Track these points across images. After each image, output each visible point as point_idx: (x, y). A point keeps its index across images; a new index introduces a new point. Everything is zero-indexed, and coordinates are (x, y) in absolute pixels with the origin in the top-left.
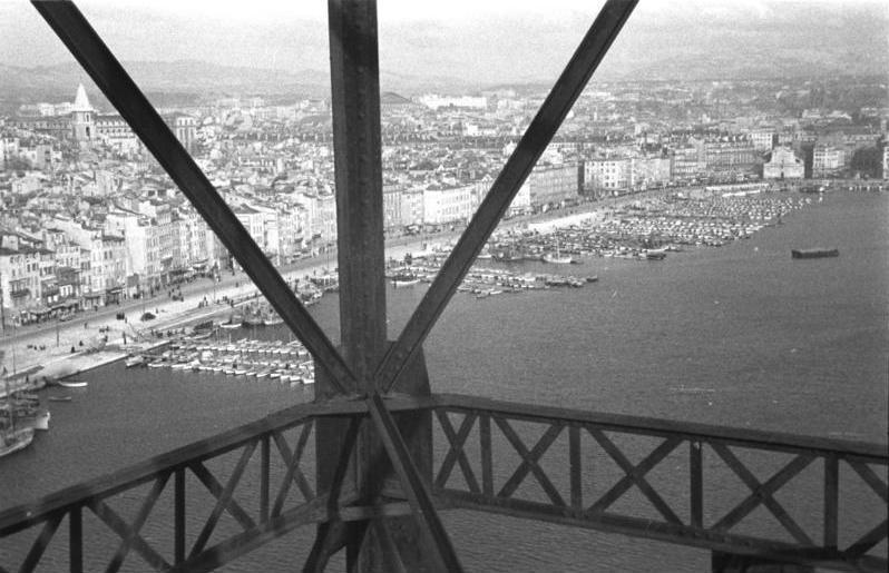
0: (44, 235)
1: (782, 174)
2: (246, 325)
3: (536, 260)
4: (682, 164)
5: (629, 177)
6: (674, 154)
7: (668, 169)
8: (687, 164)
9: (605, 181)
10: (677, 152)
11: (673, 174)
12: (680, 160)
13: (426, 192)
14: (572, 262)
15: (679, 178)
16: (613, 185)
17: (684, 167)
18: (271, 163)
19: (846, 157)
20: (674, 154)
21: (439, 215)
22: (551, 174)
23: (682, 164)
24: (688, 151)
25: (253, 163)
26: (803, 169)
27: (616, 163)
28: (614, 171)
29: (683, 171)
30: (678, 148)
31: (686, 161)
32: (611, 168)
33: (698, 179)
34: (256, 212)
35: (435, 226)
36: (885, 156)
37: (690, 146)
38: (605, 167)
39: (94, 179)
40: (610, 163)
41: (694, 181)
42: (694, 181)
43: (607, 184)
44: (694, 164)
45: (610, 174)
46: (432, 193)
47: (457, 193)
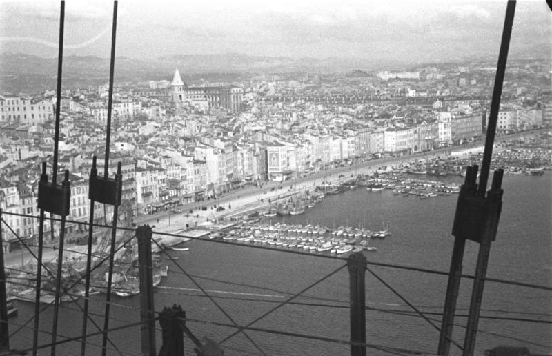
3: (456, 175)
5: (516, 122)
7: (541, 117)
10: (547, 105)
13: (386, 133)
16: (505, 127)
18: (289, 115)
20: (545, 107)
27: (507, 113)
28: (505, 118)
32: (503, 116)
34: (282, 145)
39: (185, 126)
40: (503, 113)
43: (501, 127)
45: (503, 120)
46: (390, 133)
47: (405, 133)
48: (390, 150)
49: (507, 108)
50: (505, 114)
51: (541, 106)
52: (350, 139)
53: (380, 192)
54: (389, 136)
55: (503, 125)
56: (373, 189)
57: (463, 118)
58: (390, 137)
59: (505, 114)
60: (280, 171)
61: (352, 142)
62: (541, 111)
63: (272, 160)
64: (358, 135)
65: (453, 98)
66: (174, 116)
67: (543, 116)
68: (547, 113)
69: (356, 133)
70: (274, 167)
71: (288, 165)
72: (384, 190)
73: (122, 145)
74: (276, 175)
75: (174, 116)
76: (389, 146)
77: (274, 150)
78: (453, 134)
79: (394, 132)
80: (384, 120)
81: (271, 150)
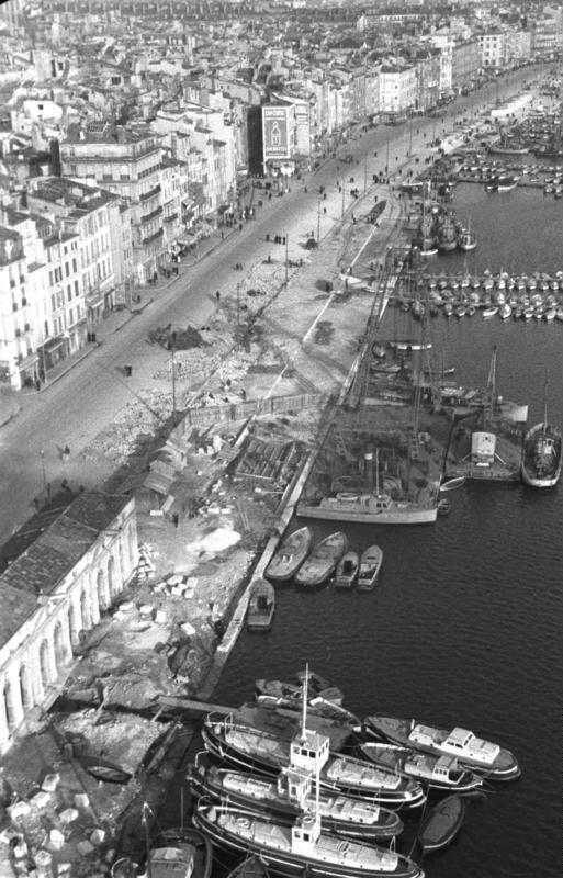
0: (173, 142)
2: (442, 253)
4: (542, 37)
6: (535, 26)
7: (528, 43)
8: (546, 37)
9: (484, 59)
10: (538, 23)
11: (534, 49)
12: (540, 33)
13: (382, 75)
15: (539, 53)
16: (494, 62)
17: (544, 40)
18: (180, 41)
20: (535, 26)
21: (397, 102)
22: (463, 49)
23: (542, 37)
24: (548, 22)
25: (158, 41)
28: (495, 46)
29: (542, 45)
30: (538, 19)
31: (546, 33)
32: (491, 42)
33: (556, 54)
34: (289, 104)
35: (391, 115)
36: (296, 5)
37: (548, 17)
38: (485, 42)
39: (31, 62)
40: (491, 37)
41: (552, 56)
42: (552, 56)
44: (553, 36)
45: (491, 50)
48: (388, 109)
50: (495, 39)
51: (529, 25)
52: (345, 89)
53: (509, 192)
54: (386, 81)
55: (490, 59)
56: (500, 188)
57: (463, 45)
58: (389, 85)
59: (495, 39)
60: (288, 157)
61: (347, 95)
62: (529, 34)
63: (273, 136)
64: (352, 79)
65: (374, 11)
66: (81, 199)
67: (532, 42)
68: (537, 37)
69: (351, 76)
70: (275, 149)
71: (296, 143)
72: (515, 189)
73: (41, 107)
74: (283, 164)
75: (81, 199)
76: (387, 101)
77: (278, 113)
78: (454, 76)
79: (397, 75)
80: (349, 51)
81: (270, 113)
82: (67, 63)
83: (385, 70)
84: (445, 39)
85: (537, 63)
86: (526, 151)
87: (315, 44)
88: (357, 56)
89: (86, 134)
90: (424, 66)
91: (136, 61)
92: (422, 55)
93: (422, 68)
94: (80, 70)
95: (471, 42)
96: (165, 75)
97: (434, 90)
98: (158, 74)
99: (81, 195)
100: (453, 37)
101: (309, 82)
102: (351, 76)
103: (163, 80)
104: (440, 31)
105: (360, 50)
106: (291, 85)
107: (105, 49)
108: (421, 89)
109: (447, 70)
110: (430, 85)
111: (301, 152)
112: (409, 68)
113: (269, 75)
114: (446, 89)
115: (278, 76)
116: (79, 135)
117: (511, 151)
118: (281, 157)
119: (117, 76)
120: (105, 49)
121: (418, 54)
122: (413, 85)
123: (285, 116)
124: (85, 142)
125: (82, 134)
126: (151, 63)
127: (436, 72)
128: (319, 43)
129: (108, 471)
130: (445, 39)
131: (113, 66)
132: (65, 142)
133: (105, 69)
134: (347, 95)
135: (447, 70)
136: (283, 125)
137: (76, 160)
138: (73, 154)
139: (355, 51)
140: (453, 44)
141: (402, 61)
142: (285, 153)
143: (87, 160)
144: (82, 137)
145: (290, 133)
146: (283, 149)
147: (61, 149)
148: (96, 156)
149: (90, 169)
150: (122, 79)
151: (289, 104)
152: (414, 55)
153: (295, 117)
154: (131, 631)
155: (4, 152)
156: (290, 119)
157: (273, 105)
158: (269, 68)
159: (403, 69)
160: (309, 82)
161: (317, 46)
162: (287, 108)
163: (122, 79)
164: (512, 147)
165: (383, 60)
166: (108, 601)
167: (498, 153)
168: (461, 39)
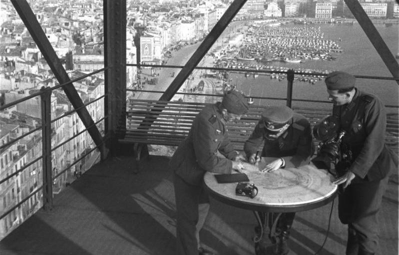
1: (272, 15)
14: (301, 62)
18: (88, 7)
19: (297, 8)
26: (281, 13)
33: (244, 17)
34: (152, 36)
42: (243, 18)
49: (220, 6)
52: (169, 30)
60: (152, 60)
64: (171, 26)
70: (146, 56)
77: (148, 41)
82: (42, 16)
83: (183, 22)
84: (205, 9)
85: (237, 21)
86: (253, 59)
87: (146, 9)
88: (168, 16)
89: (85, 51)
90: (198, 21)
91: (73, 15)
92: (198, 16)
93: (197, 22)
94: (49, 19)
95: (214, 11)
96: (87, 22)
97: (202, 31)
98: (83, 21)
99: (91, 80)
100: (208, 9)
101: (158, 27)
102: (171, 24)
103: (86, 24)
104: (201, 6)
105: (169, 13)
106: (151, 28)
107: (57, 10)
108: (197, 31)
109: (206, 22)
110: (201, 29)
111: (157, 58)
112: (193, 22)
113: (134, 23)
114: (206, 31)
115: (139, 24)
116: (82, 51)
117: (245, 59)
118: (148, 60)
119: (68, 22)
120: (57, 10)
121: (196, 15)
122: (194, 29)
123: (151, 42)
124: (85, 54)
125: (83, 51)
126: (80, 16)
127: (202, 24)
128: (148, 9)
129: (99, 158)
130: (205, 9)
131: (63, 17)
132: (75, 54)
133: (61, 19)
134: (170, 33)
135: (206, 22)
136: (150, 45)
137: (80, 63)
138: (79, 60)
139: (167, 13)
140: (208, 12)
141: (189, 18)
142: (151, 58)
143: (86, 63)
144: (84, 52)
145: (152, 49)
146: (149, 56)
147: (73, 58)
148: (91, 61)
149: (87, 67)
150: (70, 24)
151: (152, 36)
152: (194, 16)
153: (154, 42)
154: (63, 172)
155: (38, 58)
156: (153, 43)
157: (146, 37)
158: (134, 20)
159: (191, 22)
160: (158, 27)
161: (147, 10)
162: (152, 38)
163: (70, 24)
164: (247, 58)
165: (182, 18)
166: (5, 142)
167: (241, 60)
168: (210, 10)
